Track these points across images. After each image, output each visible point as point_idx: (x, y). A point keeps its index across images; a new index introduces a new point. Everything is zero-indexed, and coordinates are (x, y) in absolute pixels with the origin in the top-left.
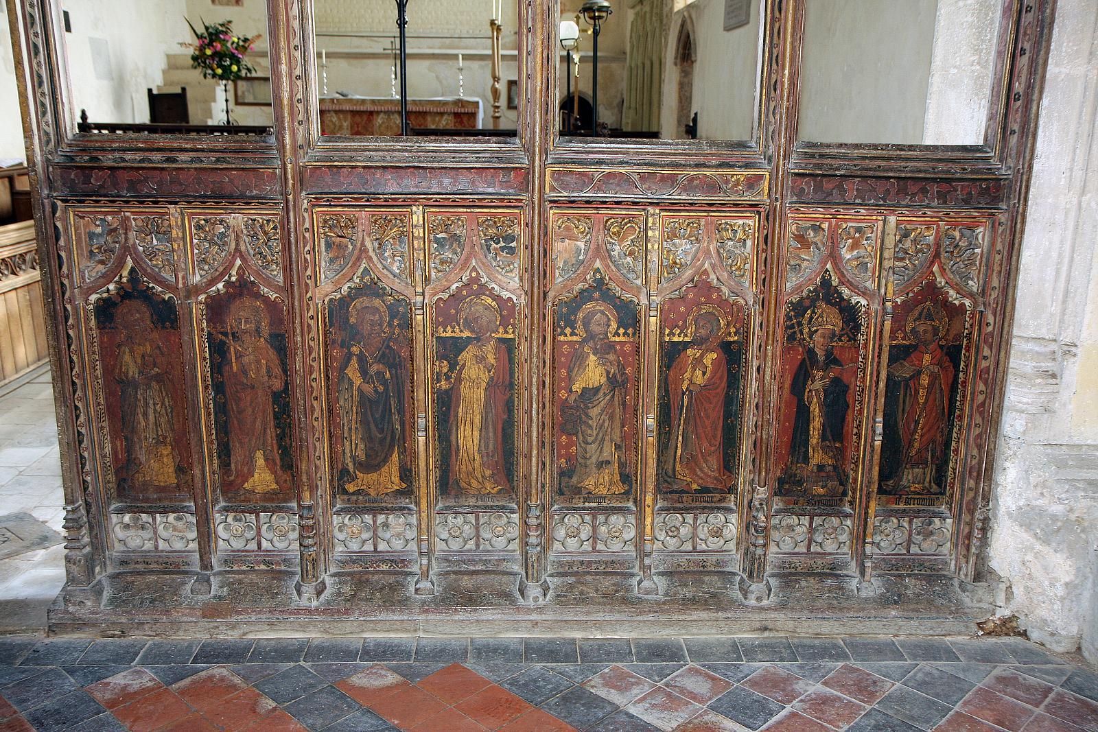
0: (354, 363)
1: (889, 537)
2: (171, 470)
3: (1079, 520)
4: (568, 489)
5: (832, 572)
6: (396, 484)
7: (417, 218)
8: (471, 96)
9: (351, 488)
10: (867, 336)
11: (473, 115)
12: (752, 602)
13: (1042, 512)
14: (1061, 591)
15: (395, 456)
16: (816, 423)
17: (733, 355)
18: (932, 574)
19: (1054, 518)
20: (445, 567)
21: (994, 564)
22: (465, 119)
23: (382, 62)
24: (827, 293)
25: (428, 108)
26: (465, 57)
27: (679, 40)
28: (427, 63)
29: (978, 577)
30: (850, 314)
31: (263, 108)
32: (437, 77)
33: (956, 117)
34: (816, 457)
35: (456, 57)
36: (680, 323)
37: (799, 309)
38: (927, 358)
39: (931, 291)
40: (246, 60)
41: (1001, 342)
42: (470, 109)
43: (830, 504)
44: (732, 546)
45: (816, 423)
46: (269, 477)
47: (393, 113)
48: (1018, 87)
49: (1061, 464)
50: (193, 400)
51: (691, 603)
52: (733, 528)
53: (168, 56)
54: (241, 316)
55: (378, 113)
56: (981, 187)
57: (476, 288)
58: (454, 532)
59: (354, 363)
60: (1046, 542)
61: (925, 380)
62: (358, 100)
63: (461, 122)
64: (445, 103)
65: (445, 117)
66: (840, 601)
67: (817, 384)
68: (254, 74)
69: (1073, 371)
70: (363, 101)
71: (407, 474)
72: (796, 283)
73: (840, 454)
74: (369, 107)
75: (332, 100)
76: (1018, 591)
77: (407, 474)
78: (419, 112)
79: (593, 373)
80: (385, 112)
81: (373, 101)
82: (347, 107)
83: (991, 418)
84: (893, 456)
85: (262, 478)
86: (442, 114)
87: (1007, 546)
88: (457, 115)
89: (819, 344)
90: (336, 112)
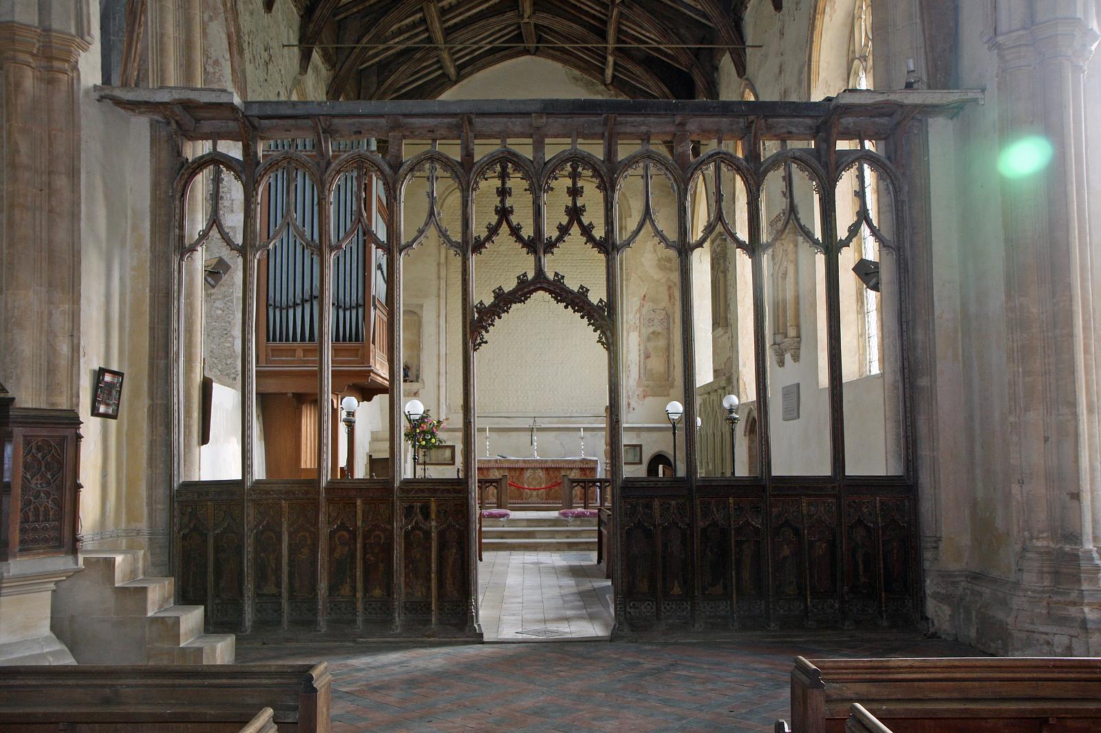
0: (709, 549)
2: (646, 587)
3: (951, 595)
7: (731, 500)
8: (590, 456)
9: (707, 593)
11: (594, 469)
12: (846, 627)
13: (939, 593)
14: (948, 618)
15: (721, 582)
19: (943, 595)
22: (588, 472)
23: (522, 434)
25: (562, 465)
26: (585, 429)
27: (747, 422)
28: (553, 434)
29: (922, 618)
31: (436, 467)
32: (561, 444)
34: (862, 580)
35: (578, 429)
38: (895, 544)
40: (441, 435)
42: (592, 465)
44: (837, 612)
46: (679, 589)
47: (537, 468)
48: (910, 458)
49: (943, 577)
53: (372, 432)
55: (527, 469)
57: (747, 524)
59: (709, 549)
60: (941, 603)
61: (895, 551)
62: (514, 460)
63: (585, 474)
64: (575, 461)
65: (574, 471)
68: (444, 444)
69: (942, 545)
70: (518, 461)
74: (521, 465)
75: (496, 461)
76: (936, 622)
77: (725, 588)
78: (556, 468)
79: (786, 551)
80: (532, 468)
81: (524, 461)
82: (506, 465)
85: (677, 590)
86: (571, 469)
87: (931, 606)
88: (582, 469)
90: (497, 468)
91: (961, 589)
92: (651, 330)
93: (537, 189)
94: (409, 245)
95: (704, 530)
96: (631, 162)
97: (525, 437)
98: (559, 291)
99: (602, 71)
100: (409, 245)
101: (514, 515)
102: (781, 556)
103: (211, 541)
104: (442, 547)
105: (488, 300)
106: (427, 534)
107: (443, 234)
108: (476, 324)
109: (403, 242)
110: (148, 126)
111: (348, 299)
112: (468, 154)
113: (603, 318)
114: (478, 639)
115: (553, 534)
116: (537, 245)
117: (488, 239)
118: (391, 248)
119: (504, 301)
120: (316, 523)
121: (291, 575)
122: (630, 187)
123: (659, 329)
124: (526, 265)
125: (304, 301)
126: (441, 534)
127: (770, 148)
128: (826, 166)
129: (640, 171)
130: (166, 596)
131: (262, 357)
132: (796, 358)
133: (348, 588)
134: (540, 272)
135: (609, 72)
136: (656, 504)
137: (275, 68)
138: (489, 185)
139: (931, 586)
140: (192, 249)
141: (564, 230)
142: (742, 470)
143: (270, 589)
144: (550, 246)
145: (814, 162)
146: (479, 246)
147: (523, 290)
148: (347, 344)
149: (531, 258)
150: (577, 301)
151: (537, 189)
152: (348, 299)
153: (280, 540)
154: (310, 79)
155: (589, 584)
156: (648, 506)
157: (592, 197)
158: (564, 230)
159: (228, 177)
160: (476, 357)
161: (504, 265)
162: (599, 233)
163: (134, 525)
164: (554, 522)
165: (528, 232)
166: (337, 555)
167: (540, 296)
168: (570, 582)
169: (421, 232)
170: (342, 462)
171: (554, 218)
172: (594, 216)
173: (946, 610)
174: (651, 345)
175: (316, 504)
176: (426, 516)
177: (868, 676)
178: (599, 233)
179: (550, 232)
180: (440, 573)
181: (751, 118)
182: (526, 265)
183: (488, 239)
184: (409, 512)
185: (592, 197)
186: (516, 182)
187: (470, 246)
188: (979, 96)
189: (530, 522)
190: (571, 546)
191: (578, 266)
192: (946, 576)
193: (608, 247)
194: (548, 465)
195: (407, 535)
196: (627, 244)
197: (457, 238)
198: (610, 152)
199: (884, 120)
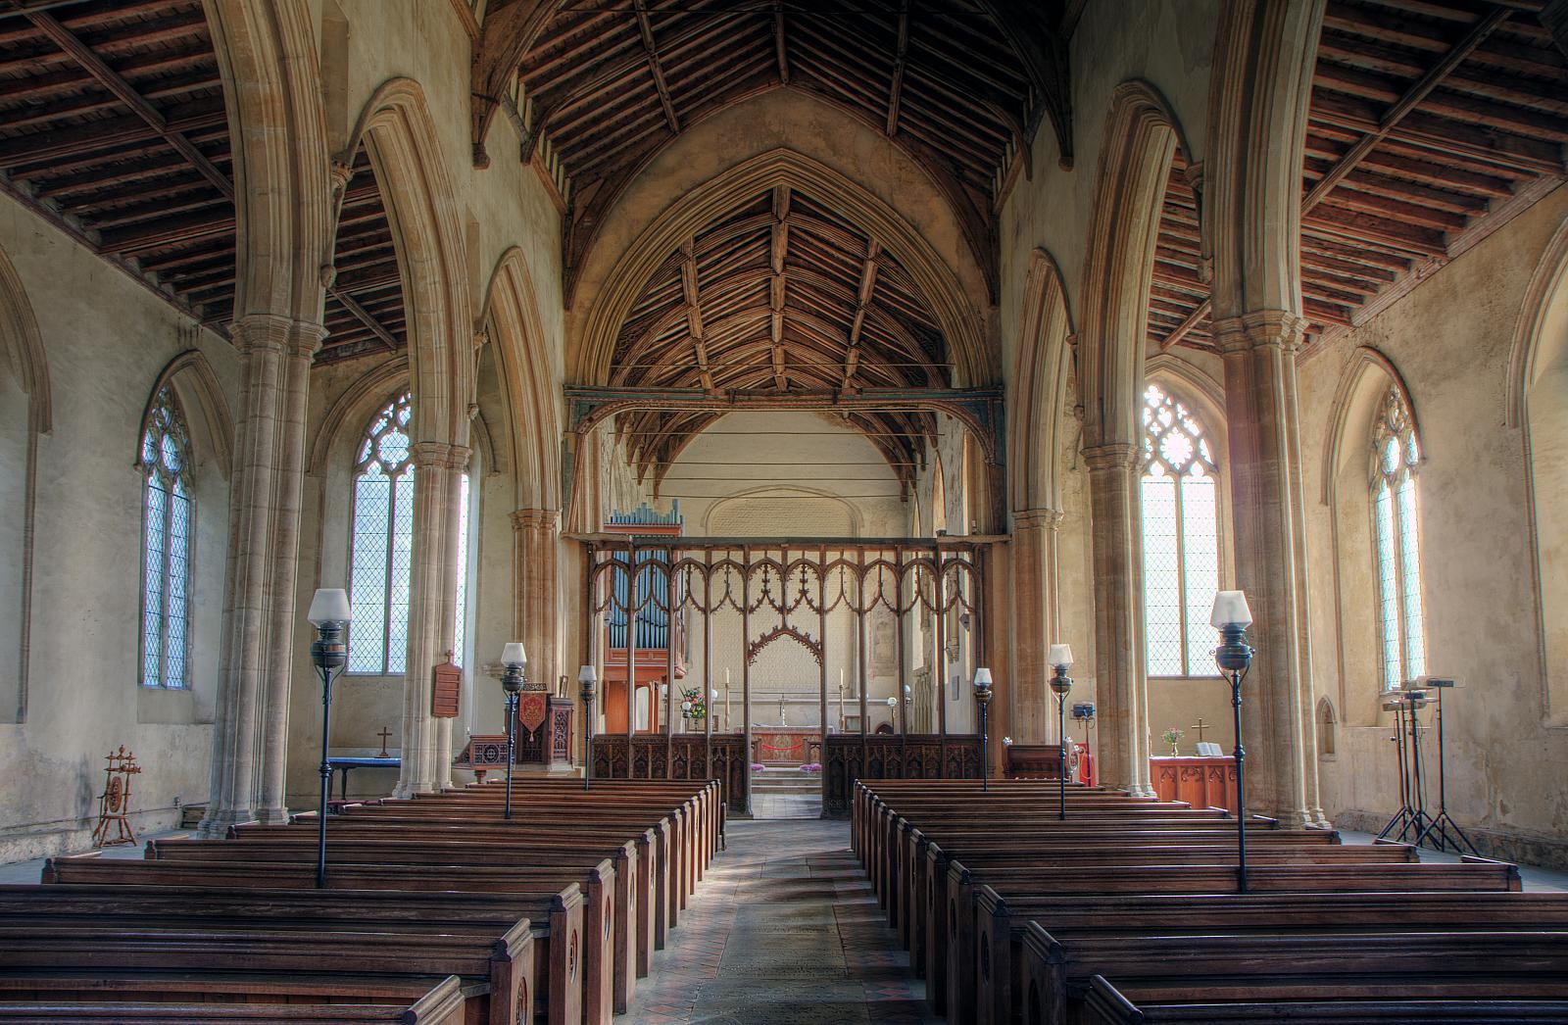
28: (798, 707)
92: (880, 621)
93: (784, 580)
94: (716, 609)
96: (834, 564)
97: (775, 709)
98: (794, 634)
99: (884, 122)
100: (716, 609)
102: (178, 480)
105: (758, 640)
106: (725, 763)
107: (733, 603)
108: (750, 652)
109: (712, 607)
112: (746, 559)
113: (819, 650)
114: (751, 817)
116: (783, 610)
117: (758, 606)
118: (706, 611)
119: (765, 639)
120: (665, 756)
122: (833, 578)
123: (887, 621)
124: (776, 620)
126: (732, 763)
127: (944, 556)
128: (937, 568)
129: (839, 570)
131: (607, 658)
132: (957, 660)
134: (784, 625)
135: (891, 119)
136: (845, 749)
138: (759, 575)
140: (600, 609)
141: (798, 602)
142: (935, 730)
144: (790, 610)
145: (931, 566)
146: (752, 610)
147: (776, 633)
148: (661, 650)
149: (780, 616)
150: (804, 640)
151: (784, 580)
153: (647, 765)
154: (619, 446)
156: (842, 749)
157: (813, 586)
158: (798, 602)
160: (750, 669)
161: (764, 621)
162: (816, 604)
164: (797, 774)
165: (778, 603)
167: (785, 636)
169: (722, 602)
170: (661, 722)
171: (793, 595)
172: (814, 594)
174: (881, 633)
175: (666, 746)
176: (724, 754)
177: (1189, 990)
178: (816, 604)
179: (790, 603)
180: (731, 783)
182: (776, 620)
183: (758, 606)
184: (715, 752)
185: (813, 586)
186: (773, 575)
187: (746, 610)
190: (808, 791)
191: (803, 620)
193: (821, 611)
194: (794, 732)
195: (692, 763)
196: (831, 609)
197: (740, 604)
198: (823, 559)
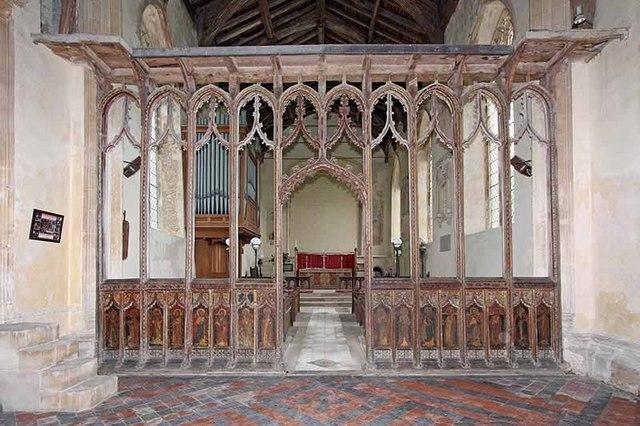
1: (541, 354)
4: (470, 346)
5: (250, 362)
6: (433, 344)
10: (531, 313)
16: (521, 331)
17: (502, 317)
18: (550, 361)
20: (532, 306)
21: (565, 359)
24: (521, 305)
30: (526, 309)
33: (541, 271)
36: (400, 252)
37: (515, 308)
39: (542, 304)
41: (560, 313)
43: (526, 348)
45: (521, 331)
50: (108, 336)
51: (499, 368)
52: (506, 353)
54: (403, 310)
56: (550, 284)
58: (446, 354)
66: (532, 367)
67: (521, 323)
71: (435, 342)
72: (515, 303)
73: (527, 337)
77: (435, 342)
83: (560, 328)
84: (539, 337)
85: (405, 343)
87: (567, 355)
89: (520, 315)
91: (589, 346)
95: (422, 310)
101: (315, 291)
103: (122, 315)
104: (261, 317)
106: (252, 311)
110: (83, 72)
111: (221, 188)
115: (332, 300)
121: (170, 334)
125: (211, 195)
130: (68, 353)
133: (204, 340)
137: (156, 29)
139: (566, 342)
143: (157, 341)
152: (221, 188)
155: (348, 324)
159: (133, 104)
163: (325, 279)
166: (198, 322)
168: (339, 325)
173: (581, 358)
181: (460, 57)
188: (624, 32)
189: (322, 295)
192: (578, 337)
199: (543, 64)
